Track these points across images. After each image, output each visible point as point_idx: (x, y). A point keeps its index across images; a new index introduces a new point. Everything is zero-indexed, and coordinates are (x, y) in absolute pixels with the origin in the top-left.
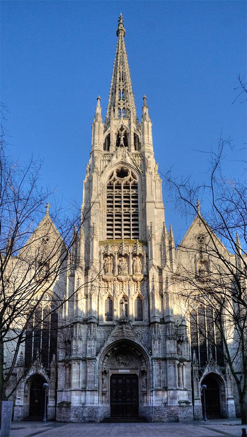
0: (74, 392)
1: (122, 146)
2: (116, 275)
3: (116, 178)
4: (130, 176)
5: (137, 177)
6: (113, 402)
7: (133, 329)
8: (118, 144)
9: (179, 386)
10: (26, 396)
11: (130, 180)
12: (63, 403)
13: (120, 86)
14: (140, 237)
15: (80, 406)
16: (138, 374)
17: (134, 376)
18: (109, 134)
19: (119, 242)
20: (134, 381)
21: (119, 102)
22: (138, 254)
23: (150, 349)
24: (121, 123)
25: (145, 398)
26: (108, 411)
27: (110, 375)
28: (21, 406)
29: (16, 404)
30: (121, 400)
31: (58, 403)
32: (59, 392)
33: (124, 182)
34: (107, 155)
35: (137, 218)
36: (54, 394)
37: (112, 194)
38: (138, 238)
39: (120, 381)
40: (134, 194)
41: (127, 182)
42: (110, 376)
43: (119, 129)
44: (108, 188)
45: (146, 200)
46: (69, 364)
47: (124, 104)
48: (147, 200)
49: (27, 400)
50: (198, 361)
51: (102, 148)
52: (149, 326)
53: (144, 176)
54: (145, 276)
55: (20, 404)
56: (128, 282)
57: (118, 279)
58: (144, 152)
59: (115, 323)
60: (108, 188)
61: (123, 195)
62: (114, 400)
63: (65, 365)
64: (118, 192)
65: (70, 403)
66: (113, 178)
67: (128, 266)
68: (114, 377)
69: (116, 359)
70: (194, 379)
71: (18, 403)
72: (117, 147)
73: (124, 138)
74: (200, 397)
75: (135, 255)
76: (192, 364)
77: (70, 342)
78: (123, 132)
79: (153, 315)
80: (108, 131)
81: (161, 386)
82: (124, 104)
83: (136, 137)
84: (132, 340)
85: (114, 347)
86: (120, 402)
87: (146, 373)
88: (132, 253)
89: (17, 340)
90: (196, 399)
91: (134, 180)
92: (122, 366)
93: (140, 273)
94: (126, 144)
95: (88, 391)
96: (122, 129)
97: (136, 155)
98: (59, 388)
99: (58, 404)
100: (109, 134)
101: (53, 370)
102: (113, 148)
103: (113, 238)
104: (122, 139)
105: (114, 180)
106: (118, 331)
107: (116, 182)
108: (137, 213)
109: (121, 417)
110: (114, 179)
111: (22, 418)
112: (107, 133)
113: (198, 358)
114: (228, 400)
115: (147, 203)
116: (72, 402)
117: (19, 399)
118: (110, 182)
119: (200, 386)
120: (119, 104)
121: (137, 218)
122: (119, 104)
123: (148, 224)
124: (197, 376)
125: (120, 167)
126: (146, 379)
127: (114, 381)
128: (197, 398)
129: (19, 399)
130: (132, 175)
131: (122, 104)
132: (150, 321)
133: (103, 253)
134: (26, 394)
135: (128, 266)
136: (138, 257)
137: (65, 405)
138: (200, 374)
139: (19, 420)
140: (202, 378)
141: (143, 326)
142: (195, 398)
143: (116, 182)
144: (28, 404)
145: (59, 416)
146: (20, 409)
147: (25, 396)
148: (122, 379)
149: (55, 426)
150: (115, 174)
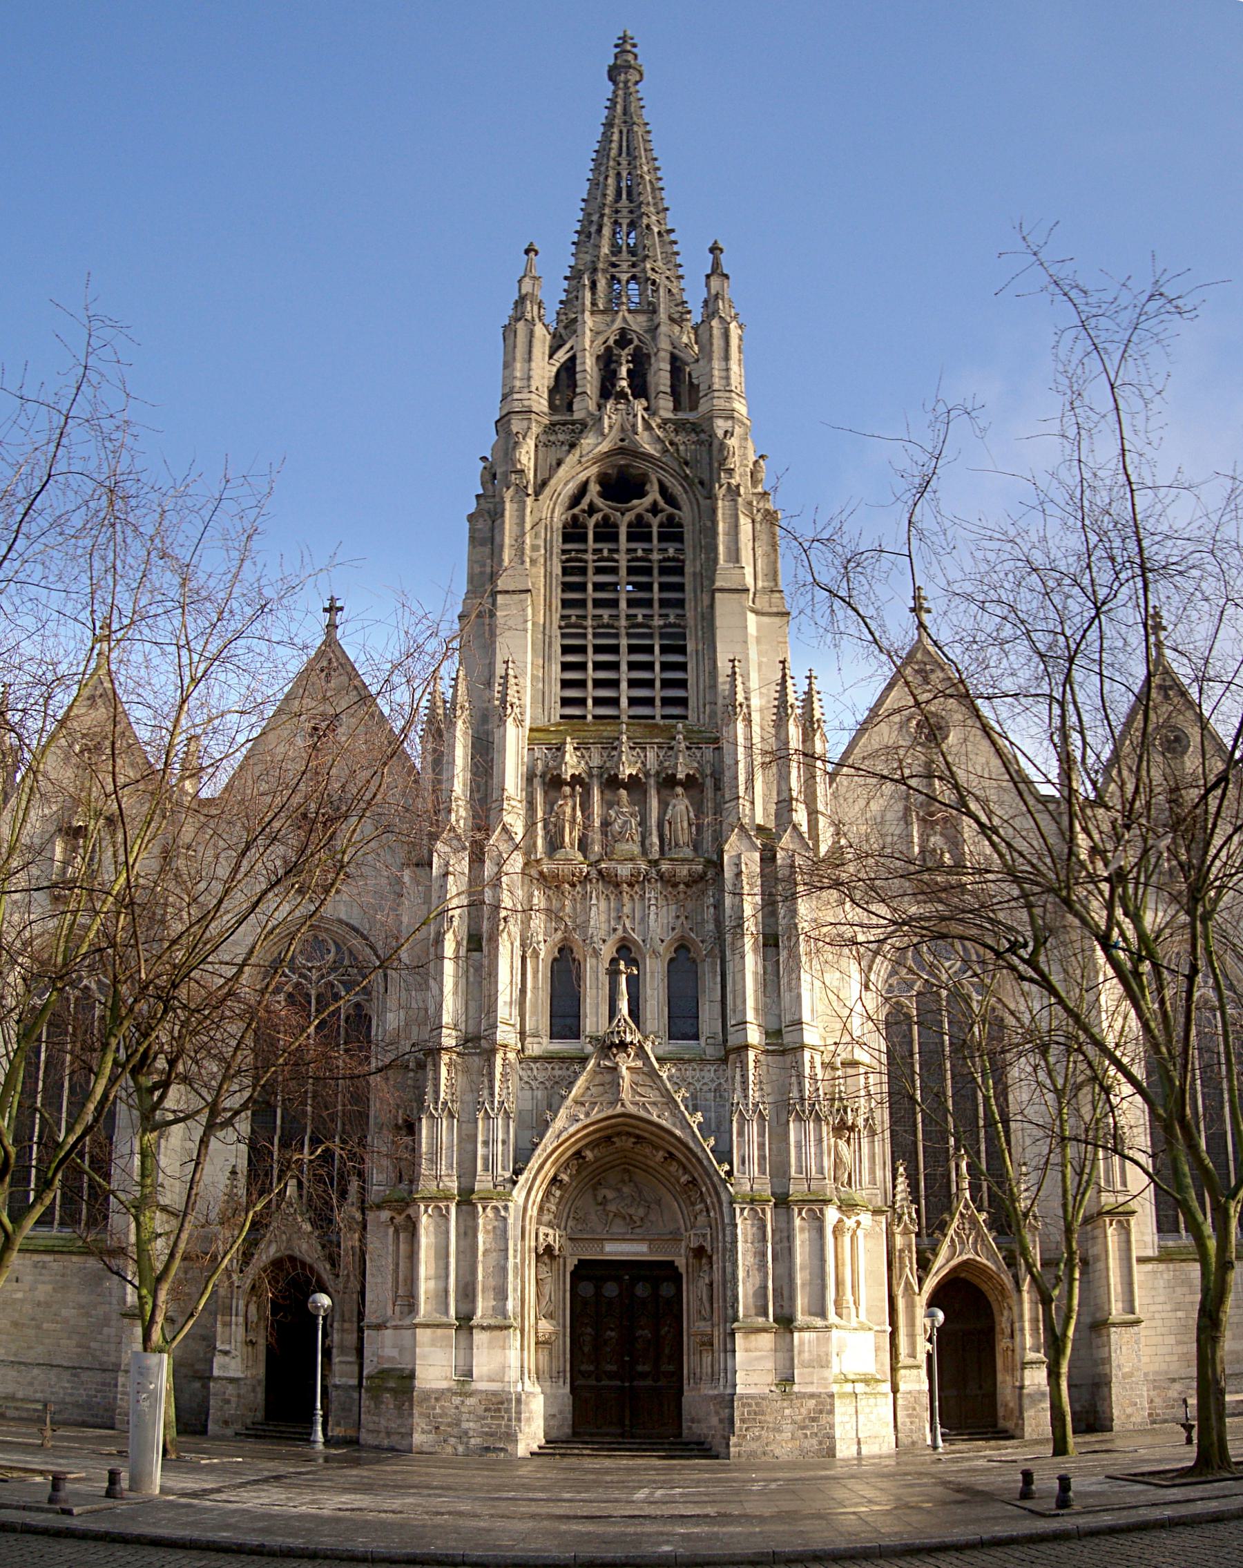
0: (429, 1331)
1: (622, 395)
2: (593, 858)
3: (599, 502)
4: (654, 495)
5: (682, 498)
6: (586, 1375)
7: (1124, 1378)
8: (607, 390)
9: (839, 1315)
10: (252, 1343)
11: (654, 509)
12: (384, 1374)
13: (617, 212)
14: (691, 714)
15: (449, 1390)
16: (680, 1262)
17: (665, 1272)
18: (573, 359)
19: (608, 730)
20: (666, 1290)
21: (614, 259)
22: (681, 776)
23: (724, 1155)
24: (618, 324)
25: (707, 1359)
26: (561, 1412)
27: (571, 1263)
28: (232, 1380)
29: (216, 1373)
30: (614, 1368)
31: (365, 1373)
32: (373, 1333)
33: (629, 517)
34: (564, 425)
35: (678, 675)
36: (352, 1339)
37: (581, 560)
38: (685, 717)
39: (611, 1290)
40: (669, 559)
41: (639, 517)
42: (570, 1268)
43: (611, 342)
44: (567, 538)
45: (713, 582)
46: (409, 1217)
47: (634, 265)
48: (719, 584)
49: (256, 1359)
50: (918, 1211)
51: (546, 403)
52: (724, 1060)
53: (710, 498)
54: (709, 863)
55: (232, 1374)
56: (643, 889)
57: (600, 872)
58: (711, 418)
59: (589, 1048)
60: (563, 591)
61: (623, 564)
62: (584, 1368)
63: (392, 1219)
64: (605, 553)
65: (412, 1376)
66: (584, 504)
67: (643, 823)
68: (586, 1272)
69: (595, 1196)
70: (899, 1291)
71: (223, 1367)
72: (602, 401)
73: (629, 371)
74: (922, 1358)
75: (668, 782)
76: (889, 1225)
77: (411, 1128)
78: (630, 349)
79: (739, 1019)
80: (567, 346)
81: (766, 1315)
82: (634, 265)
83: (677, 365)
84: (655, 1118)
85: (586, 1146)
86: (611, 1376)
87: (710, 1257)
88: (658, 773)
89: (203, 1118)
90: (905, 1367)
91: (670, 510)
92: (618, 1228)
93: (688, 852)
94: (640, 388)
95: (483, 1328)
96: (623, 339)
97: (680, 426)
98: (370, 1318)
99: (368, 1378)
100: (573, 359)
101: (350, 1241)
102: (585, 404)
103: (584, 717)
104: (623, 371)
105: (592, 509)
106: (597, 1080)
107: (598, 516)
108: (679, 626)
109: (613, 1435)
110: (591, 505)
111: (238, 1427)
112: (562, 356)
113: (916, 1200)
114: (1023, 1369)
115: (718, 595)
116: (419, 1372)
117: (226, 1353)
118: (575, 517)
119: (920, 1311)
120: (614, 265)
121: (678, 675)
122: (617, 212)
123: (723, 667)
124: (910, 1272)
125: (614, 466)
126: (711, 1284)
127: (587, 1289)
128: (910, 1361)
129: (226, 1353)
130: (663, 490)
131: (625, 266)
132: (725, 1041)
133: (543, 776)
134: (251, 1337)
135: (643, 823)
136: (679, 790)
137: (392, 1384)
138: (924, 1265)
139: (229, 1432)
140: (931, 1283)
141: (703, 1061)
142: (904, 1359)
143: (598, 516)
144: (261, 1371)
145: (371, 1426)
146: (231, 1389)
147: (246, 1343)
148: (618, 1279)
149: (357, 1463)
150: (594, 488)
